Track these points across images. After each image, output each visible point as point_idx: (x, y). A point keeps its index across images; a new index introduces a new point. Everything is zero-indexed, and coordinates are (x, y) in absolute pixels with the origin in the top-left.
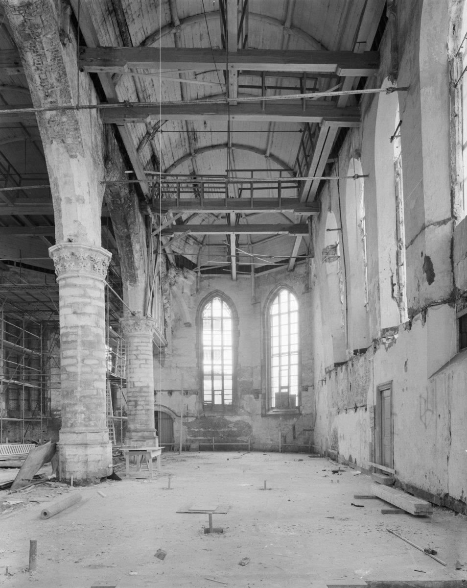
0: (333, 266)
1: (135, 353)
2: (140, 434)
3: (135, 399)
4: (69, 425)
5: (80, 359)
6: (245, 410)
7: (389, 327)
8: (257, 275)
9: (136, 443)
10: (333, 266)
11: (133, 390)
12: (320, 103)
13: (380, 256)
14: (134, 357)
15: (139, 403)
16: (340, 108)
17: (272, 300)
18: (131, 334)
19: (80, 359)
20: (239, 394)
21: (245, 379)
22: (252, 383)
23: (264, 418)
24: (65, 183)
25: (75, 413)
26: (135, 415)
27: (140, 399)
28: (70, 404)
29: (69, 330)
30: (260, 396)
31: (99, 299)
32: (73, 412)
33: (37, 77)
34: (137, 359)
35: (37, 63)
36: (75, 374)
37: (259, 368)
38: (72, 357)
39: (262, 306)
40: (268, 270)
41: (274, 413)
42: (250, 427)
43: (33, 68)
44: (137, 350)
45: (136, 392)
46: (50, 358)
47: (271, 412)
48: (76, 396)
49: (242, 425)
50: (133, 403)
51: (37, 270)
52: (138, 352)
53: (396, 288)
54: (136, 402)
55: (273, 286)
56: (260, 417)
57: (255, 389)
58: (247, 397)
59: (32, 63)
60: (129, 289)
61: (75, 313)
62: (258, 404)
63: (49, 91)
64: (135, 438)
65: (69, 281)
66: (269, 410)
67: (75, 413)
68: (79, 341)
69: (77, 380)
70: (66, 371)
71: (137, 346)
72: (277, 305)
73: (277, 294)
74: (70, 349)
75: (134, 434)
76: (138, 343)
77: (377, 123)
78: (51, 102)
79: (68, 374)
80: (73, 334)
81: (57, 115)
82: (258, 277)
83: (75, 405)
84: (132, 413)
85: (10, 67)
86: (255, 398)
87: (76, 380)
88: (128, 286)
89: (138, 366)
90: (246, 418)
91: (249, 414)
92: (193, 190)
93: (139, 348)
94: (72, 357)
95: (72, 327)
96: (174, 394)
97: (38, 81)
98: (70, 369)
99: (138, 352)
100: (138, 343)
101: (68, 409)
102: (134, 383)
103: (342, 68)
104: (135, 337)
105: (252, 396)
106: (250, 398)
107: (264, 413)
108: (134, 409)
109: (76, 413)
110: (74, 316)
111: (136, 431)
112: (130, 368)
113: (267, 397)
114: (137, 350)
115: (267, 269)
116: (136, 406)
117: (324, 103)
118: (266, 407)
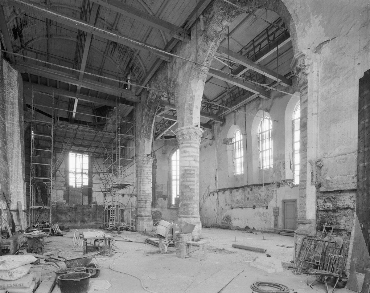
0: (230, 147)
1: (146, 175)
2: (147, 218)
3: (146, 199)
4: (190, 214)
5: (196, 182)
6: (159, 206)
7: (289, 179)
8: (165, 140)
9: (146, 222)
10: (230, 147)
11: (144, 195)
12: (259, 87)
13: (285, 152)
14: (146, 178)
15: (147, 201)
16: (265, 92)
17: (173, 153)
18: (144, 165)
19: (196, 182)
20: (156, 197)
21: (159, 190)
22: (162, 192)
23: (169, 210)
24: (198, 99)
25: (193, 208)
26: (145, 207)
27: (148, 200)
28: (191, 204)
29: (191, 168)
30: (167, 199)
31: (197, 153)
32: (192, 208)
33: (209, 52)
34: (147, 179)
35: (213, 47)
36: (194, 189)
37: (166, 185)
38: (193, 181)
39: (168, 155)
40: (171, 138)
41: (174, 207)
42: (161, 214)
43: (211, 48)
44: (147, 174)
45: (146, 196)
46: (57, 171)
47: (172, 207)
48: (194, 200)
49: (157, 213)
50: (144, 202)
51: (46, 115)
52: (148, 175)
53: (292, 165)
54: (146, 201)
55: (174, 147)
56: (166, 209)
57: (163, 195)
58: (160, 199)
59: (211, 46)
60: (146, 142)
61: (194, 160)
62: (166, 202)
63: (210, 59)
64: (146, 220)
65: (192, 145)
66: (171, 206)
67: (193, 208)
68: (196, 174)
69: (195, 192)
70: (189, 188)
71: (147, 172)
72: (176, 156)
73: (176, 150)
74: (192, 177)
75: (144, 218)
76: (148, 170)
77: (288, 105)
78: (207, 64)
79: (191, 189)
80: (193, 170)
81: (206, 69)
82: (166, 141)
83: (193, 204)
84: (143, 206)
85: (177, 34)
86: (164, 200)
87: (194, 192)
88: (146, 141)
89: (147, 182)
90: (159, 209)
91: (161, 207)
92: (167, 97)
93: (148, 173)
94: (193, 181)
95: (193, 167)
96: (125, 196)
97: (208, 54)
98: (191, 187)
99: (148, 175)
100: (148, 170)
101: (190, 206)
102: (145, 191)
103: (283, 82)
104: (146, 167)
105: (162, 199)
106: (161, 200)
107: (169, 207)
108: (145, 204)
109: (194, 208)
110: (194, 162)
111: (146, 216)
112: (143, 183)
113: (170, 199)
114: (147, 174)
115: (170, 138)
116: (146, 203)
117: (261, 88)
118: (170, 204)
